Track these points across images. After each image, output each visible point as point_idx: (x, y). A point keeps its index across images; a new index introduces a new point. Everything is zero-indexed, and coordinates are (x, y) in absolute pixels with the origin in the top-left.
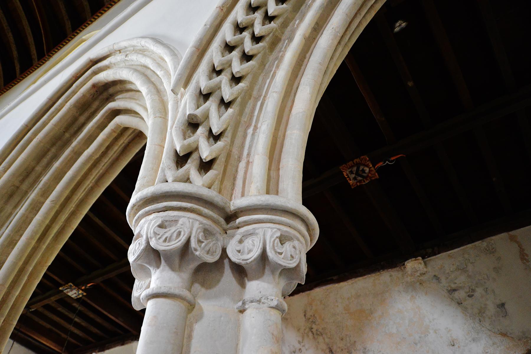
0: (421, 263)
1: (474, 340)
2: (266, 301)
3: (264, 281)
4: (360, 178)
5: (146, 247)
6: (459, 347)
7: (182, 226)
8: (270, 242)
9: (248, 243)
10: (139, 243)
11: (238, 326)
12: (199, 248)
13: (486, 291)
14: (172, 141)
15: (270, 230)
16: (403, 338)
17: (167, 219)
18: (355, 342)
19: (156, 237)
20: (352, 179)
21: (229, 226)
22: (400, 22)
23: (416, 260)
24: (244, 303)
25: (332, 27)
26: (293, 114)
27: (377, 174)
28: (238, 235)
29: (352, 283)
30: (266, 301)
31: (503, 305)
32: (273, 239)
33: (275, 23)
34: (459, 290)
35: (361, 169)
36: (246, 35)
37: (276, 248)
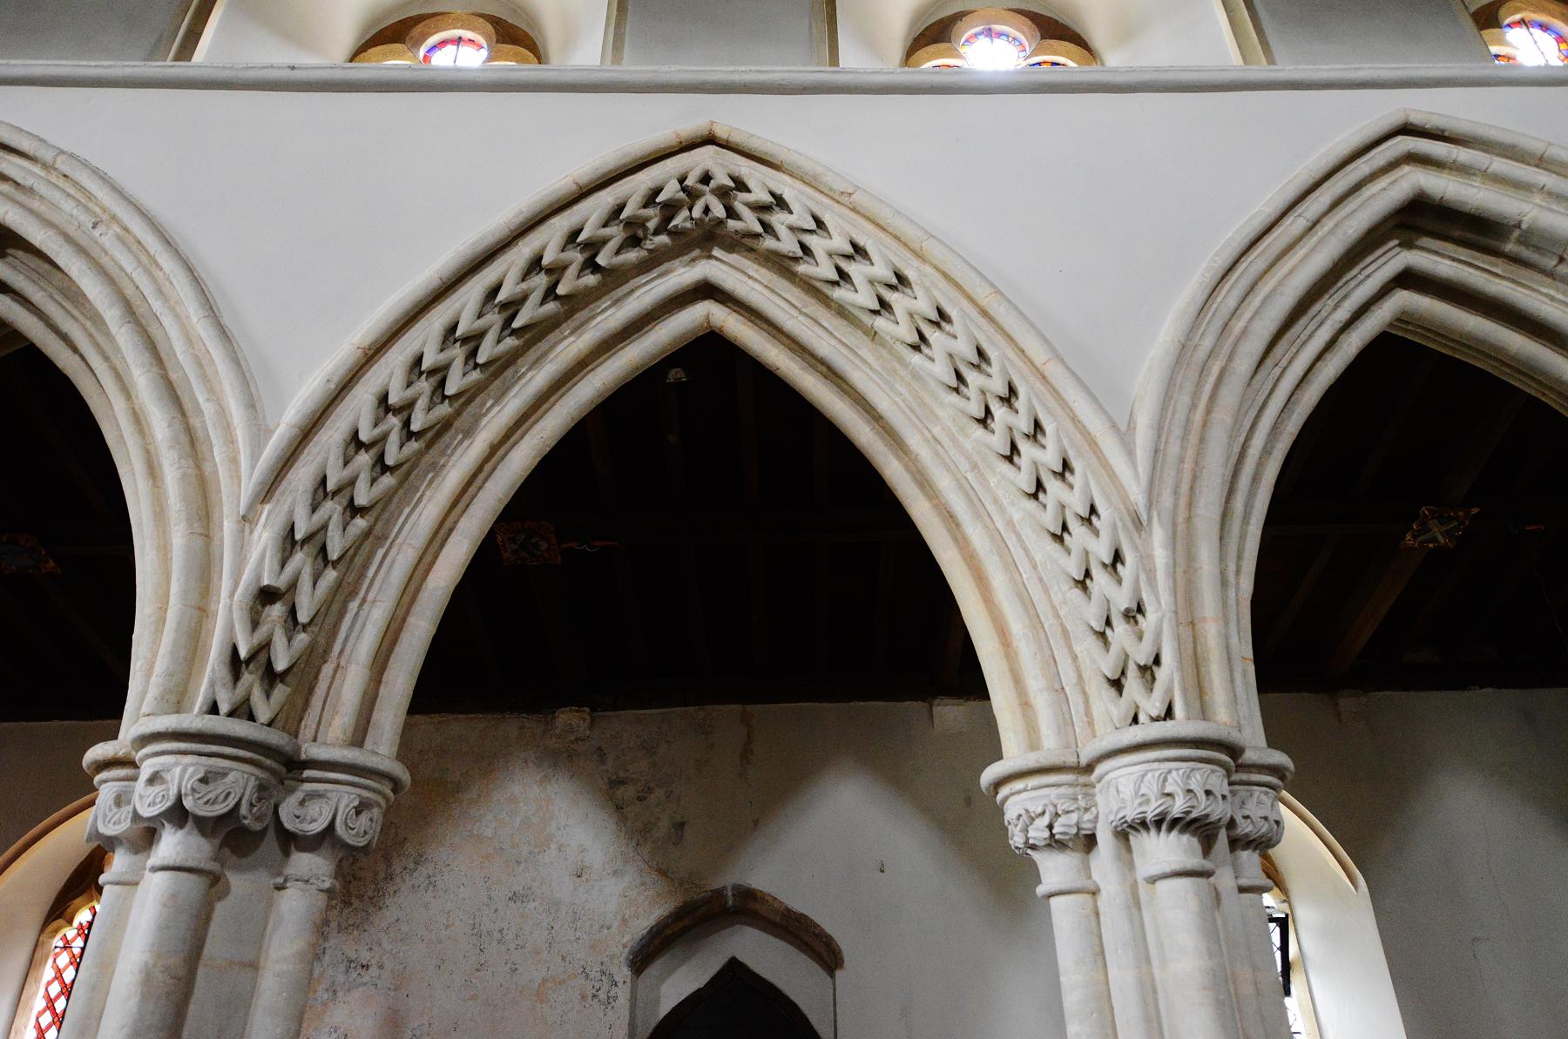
0: (584, 719)
1: (615, 873)
2: (315, 882)
3: (319, 855)
4: (524, 554)
5: (175, 804)
6: (587, 880)
7: (233, 785)
8: (343, 813)
9: (314, 809)
10: (163, 796)
11: (270, 904)
12: (249, 817)
13: (668, 797)
14: (230, 629)
15: (347, 795)
16: (501, 848)
17: (211, 770)
18: (405, 839)
19: (193, 796)
20: (509, 551)
21: (290, 775)
22: (679, 369)
23: (577, 711)
24: (286, 881)
25: (542, 435)
26: (429, 587)
27: (559, 557)
28: (300, 792)
29: (439, 722)
30: (315, 882)
31: (682, 825)
32: (348, 810)
33: (451, 407)
34: (627, 784)
35: (534, 540)
36: (395, 426)
37: (348, 821)
